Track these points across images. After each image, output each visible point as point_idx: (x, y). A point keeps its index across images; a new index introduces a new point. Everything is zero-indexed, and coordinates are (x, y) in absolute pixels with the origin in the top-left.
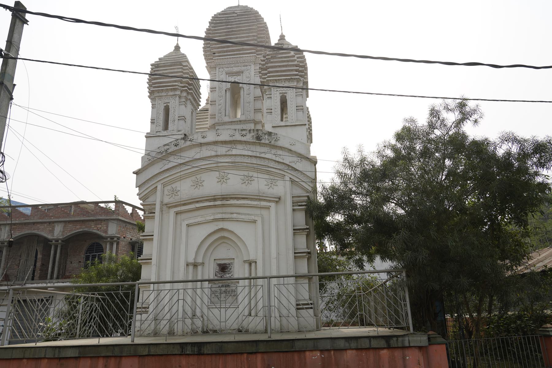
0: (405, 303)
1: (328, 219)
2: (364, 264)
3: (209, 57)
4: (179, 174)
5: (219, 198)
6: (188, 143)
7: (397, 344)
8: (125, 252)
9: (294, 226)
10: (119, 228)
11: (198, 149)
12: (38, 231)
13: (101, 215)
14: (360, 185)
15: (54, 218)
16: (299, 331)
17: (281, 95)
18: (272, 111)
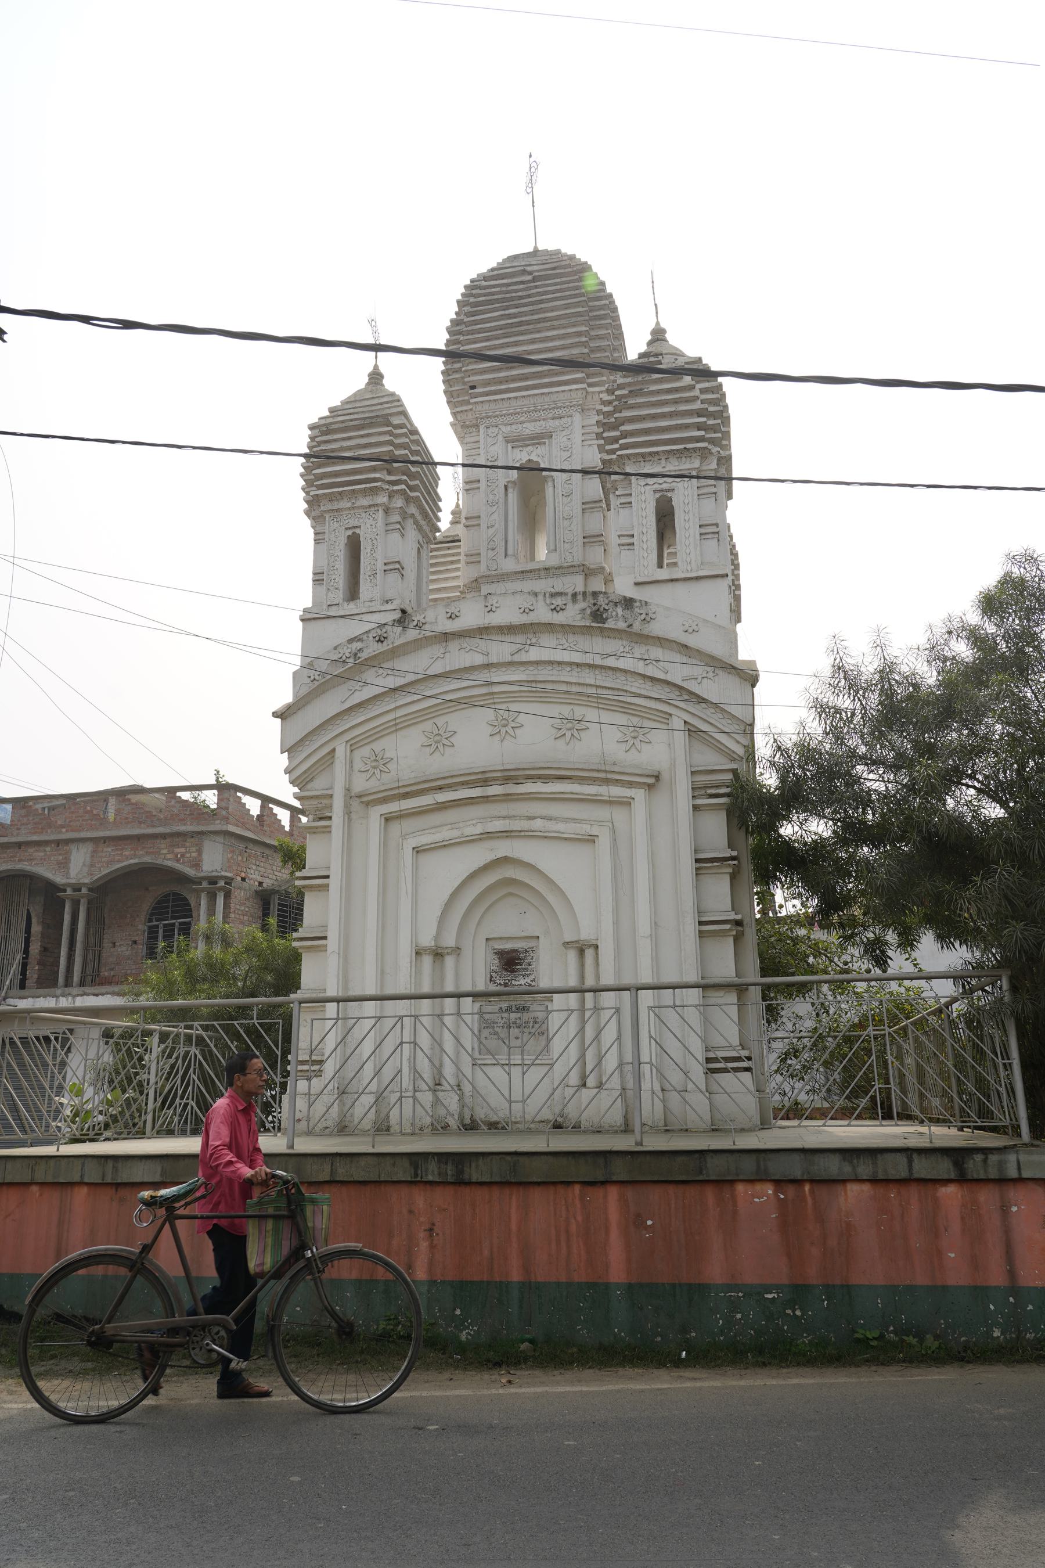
1: (787, 830)
2: (890, 953)
5: (495, 779)
6: (412, 634)
7: (986, 1171)
8: (246, 918)
9: (696, 851)
10: (230, 856)
11: (437, 650)
12: (30, 865)
13: (183, 821)
15: (67, 831)
16: (713, 1130)
17: (658, 495)
18: (635, 540)
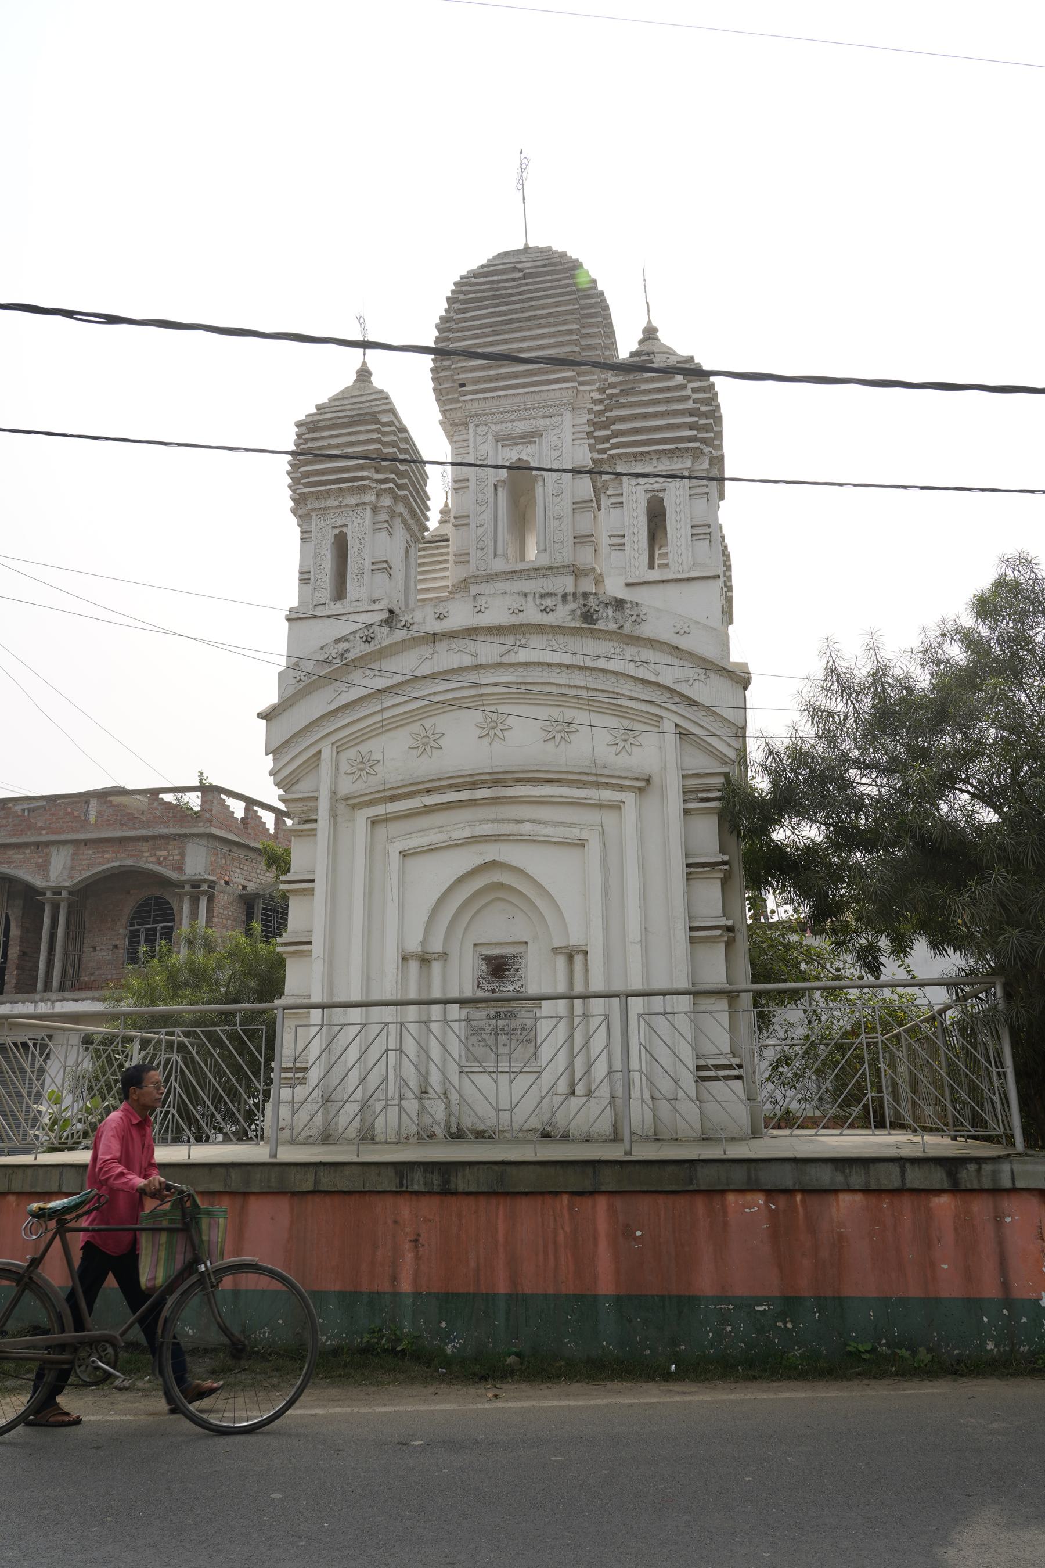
0: (1000, 1070)
1: (779, 835)
2: (883, 960)
3: (447, 394)
4: (377, 718)
5: (483, 782)
6: (400, 635)
7: (979, 1181)
8: (229, 922)
9: (687, 856)
10: (213, 859)
11: (425, 651)
14: (872, 743)
15: (47, 833)
17: (649, 495)
18: (626, 540)
